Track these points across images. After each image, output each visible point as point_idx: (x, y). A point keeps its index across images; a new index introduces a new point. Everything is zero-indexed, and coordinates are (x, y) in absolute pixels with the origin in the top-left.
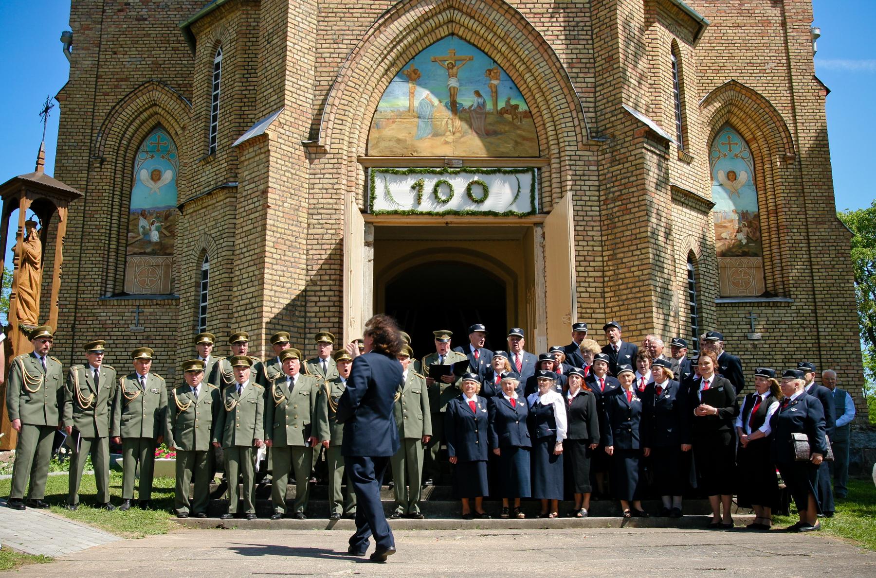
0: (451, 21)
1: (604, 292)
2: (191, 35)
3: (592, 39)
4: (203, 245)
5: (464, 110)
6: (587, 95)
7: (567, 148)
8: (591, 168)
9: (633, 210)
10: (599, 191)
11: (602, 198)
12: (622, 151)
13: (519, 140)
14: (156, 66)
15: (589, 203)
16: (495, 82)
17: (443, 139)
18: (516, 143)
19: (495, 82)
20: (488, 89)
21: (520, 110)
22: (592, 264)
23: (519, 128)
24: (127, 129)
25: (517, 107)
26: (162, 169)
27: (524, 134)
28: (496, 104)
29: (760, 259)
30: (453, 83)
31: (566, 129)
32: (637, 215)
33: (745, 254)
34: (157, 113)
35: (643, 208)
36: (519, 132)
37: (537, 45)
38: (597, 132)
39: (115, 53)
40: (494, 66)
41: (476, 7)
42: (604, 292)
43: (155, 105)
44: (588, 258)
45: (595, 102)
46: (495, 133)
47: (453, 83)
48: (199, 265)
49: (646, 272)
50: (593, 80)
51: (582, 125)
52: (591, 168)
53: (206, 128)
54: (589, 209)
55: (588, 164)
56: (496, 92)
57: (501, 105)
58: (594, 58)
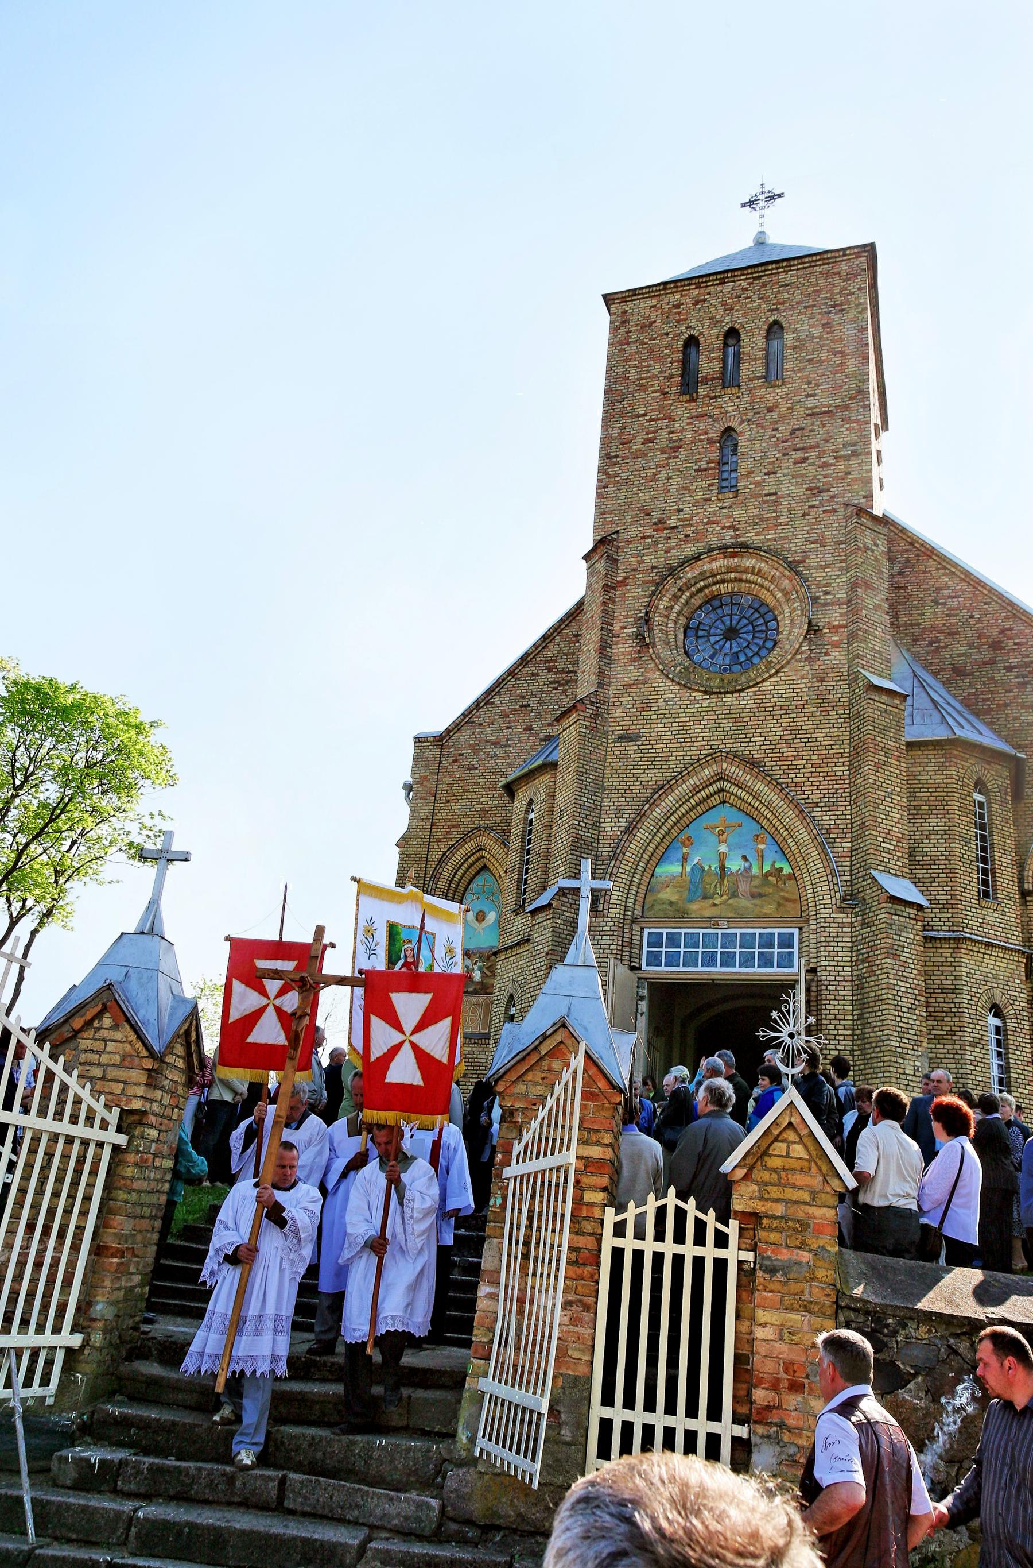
0: (722, 790)
1: (854, 1050)
2: (510, 790)
3: (850, 805)
4: (511, 991)
5: (732, 873)
6: (843, 859)
7: (822, 911)
8: (845, 930)
9: (878, 972)
10: (851, 952)
11: (854, 959)
12: (871, 914)
13: (781, 901)
14: (484, 813)
15: (842, 964)
16: (762, 847)
17: (711, 901)
18: (779, 905)
19: (762, 847)
20: (755, 854)
21: (784, 872)
22: (842, 1022)
23: (782, 890)
24: (456, 873)
26: (487, 911)
27: (786, 895)
30: (723, 848)
31: (822, 893)
32: (880, 977)
34: (483, 857)
35: (885, 971)
36: (782, 894)
37: (797, 813)
38: (851, 895)
39: (448, 802)
41: (742, 779)
42: (854, 1050)
43: (482, 849)
44: (838, 1017)
45: (851, 866)
46: (761, 895)
47: (723, 848)
48: (507, 1009)
49: (885, 1032)
50: (849, 845)
51: (836, 889)
52: (845, 930)
53: (519, 880)
54: (841, 969)
55: (842, 925)
56: (762, 856)
57: (767, 868)
58: (852, 824)
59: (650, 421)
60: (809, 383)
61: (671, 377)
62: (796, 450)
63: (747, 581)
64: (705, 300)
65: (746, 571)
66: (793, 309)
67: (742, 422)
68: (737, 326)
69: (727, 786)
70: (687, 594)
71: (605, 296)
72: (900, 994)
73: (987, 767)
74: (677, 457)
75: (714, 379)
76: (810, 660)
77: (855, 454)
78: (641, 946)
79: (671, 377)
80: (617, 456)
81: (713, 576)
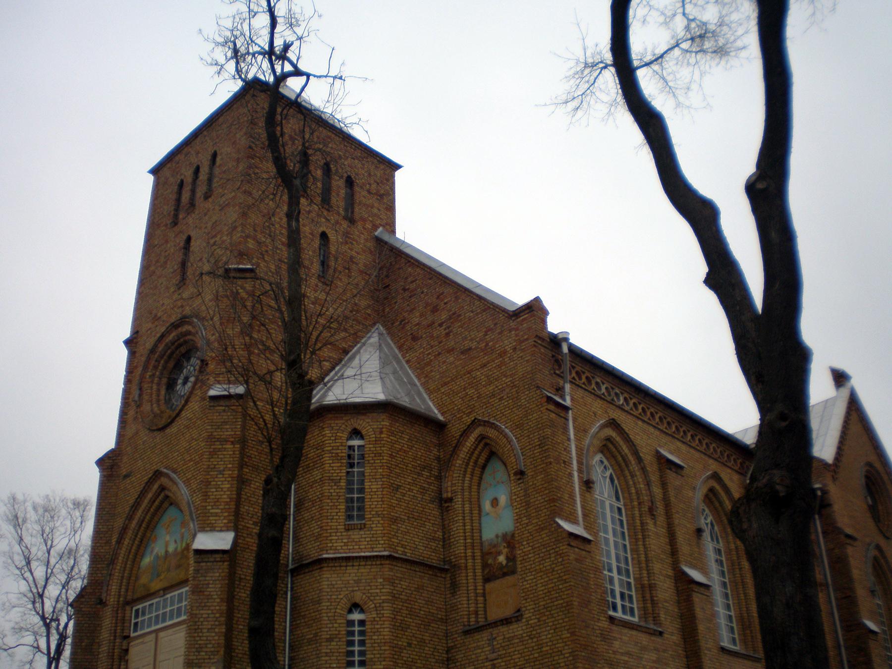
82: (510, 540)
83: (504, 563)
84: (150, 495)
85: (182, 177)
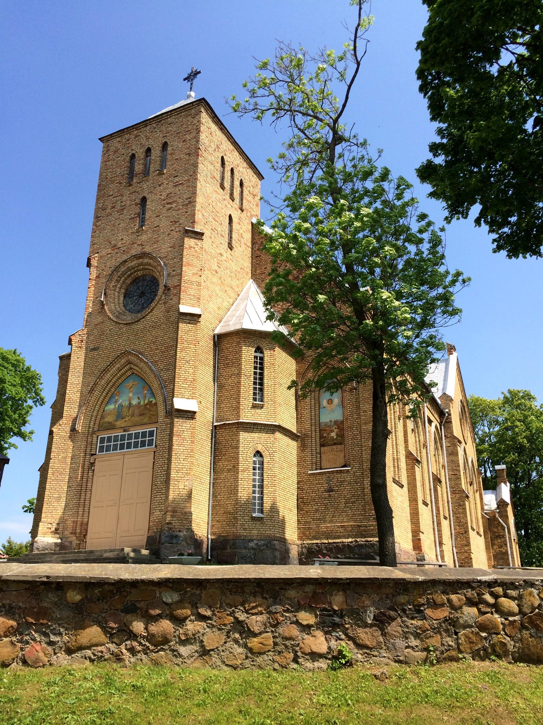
18: (150, 417)
25: (152, 401)
28: (144, 402)
29: (343, 446)
33: (335, 444)
40: (146, 385)
59: (114, 198)
60: (175, 170)
61: (124, 175)
62: (168, 204)
63: (147, 269)
64: (139, 135)
65: (145, 265)
66: (172, 135)
67: (149, 193)
68: (150, 147)
69: (132, 366)
70: (123, 278)
71: (100, 139)
72: (180, 453)
73: (264, 340)
74: (123, 214)
75: (140, 173)
76: (165, 303)
77: (190, 203)
78: (97, 444)
79: (124, 175)
80: (100, 217)
81: (134, 268)
82: (339, 425)
83: (335, 437)
84: (118, 366)
85: (134, 152)
